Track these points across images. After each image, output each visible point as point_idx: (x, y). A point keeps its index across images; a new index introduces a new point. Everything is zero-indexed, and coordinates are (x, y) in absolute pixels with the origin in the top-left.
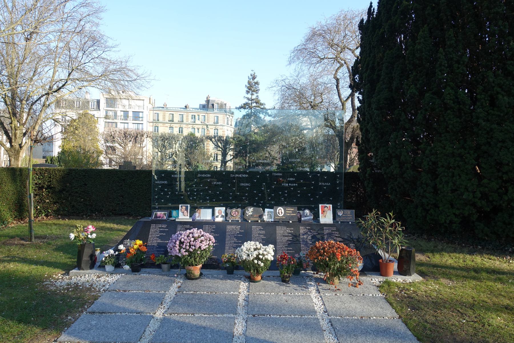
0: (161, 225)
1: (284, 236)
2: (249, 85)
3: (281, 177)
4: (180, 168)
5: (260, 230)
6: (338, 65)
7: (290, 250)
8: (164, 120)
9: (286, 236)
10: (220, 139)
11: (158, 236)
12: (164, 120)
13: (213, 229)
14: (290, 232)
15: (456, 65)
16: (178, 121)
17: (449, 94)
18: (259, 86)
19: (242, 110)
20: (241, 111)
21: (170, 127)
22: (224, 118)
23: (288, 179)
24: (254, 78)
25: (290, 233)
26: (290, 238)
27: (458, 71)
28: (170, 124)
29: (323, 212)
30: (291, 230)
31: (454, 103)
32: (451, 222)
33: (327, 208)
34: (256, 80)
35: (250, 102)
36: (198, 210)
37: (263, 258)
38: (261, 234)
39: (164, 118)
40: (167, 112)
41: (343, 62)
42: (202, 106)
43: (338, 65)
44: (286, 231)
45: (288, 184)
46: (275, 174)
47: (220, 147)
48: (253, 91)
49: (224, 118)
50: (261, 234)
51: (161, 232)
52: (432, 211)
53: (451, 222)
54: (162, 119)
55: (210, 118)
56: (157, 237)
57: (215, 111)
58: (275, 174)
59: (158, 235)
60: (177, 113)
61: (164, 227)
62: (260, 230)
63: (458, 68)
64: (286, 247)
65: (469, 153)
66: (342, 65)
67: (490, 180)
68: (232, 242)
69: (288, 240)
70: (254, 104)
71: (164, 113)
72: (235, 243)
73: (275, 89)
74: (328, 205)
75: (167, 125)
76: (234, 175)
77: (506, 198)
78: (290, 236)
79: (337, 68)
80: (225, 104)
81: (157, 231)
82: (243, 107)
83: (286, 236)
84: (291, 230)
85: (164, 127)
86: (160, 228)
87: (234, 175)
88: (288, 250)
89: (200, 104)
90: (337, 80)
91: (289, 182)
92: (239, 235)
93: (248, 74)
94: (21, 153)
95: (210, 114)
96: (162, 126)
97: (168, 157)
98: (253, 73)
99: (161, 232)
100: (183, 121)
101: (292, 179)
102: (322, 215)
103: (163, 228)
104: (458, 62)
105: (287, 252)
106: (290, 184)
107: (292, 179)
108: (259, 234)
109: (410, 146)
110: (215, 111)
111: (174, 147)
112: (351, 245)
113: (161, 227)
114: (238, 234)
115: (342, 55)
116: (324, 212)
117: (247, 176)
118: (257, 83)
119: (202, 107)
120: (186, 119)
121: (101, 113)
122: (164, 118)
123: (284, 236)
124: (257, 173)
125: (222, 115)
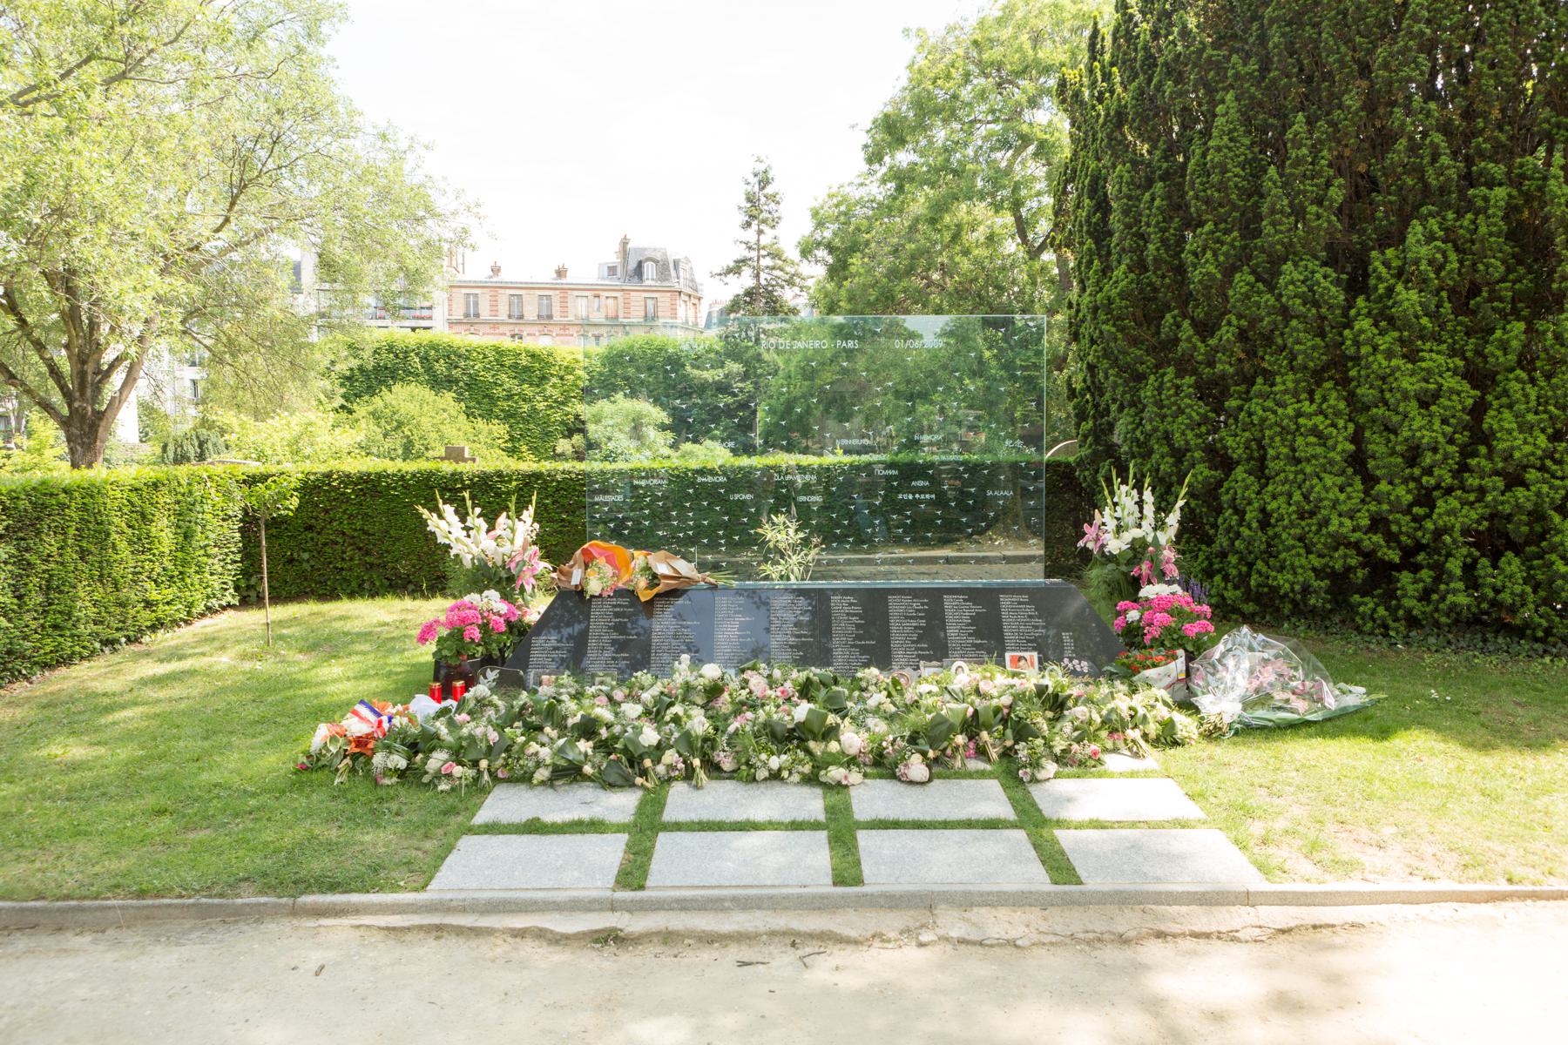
1: (906, 617)
2: (749, 205)
4: (1308, 460)
5: (850, 604)
9: (912, 618)
13: (740, 605)
15: (1313, 209)
16: (539, 316)
17: (1292, 282)
18: (781, 207)
19: (731, 278)
24: (764, 182)
26: (923, 623)
27: (1316, 223)
30: (922, 604)
31: (1304, 304)
32: (1306, 589)
34: (769, 190)
35: (754, 254)
40: (502, 291)
42: (606, 270)
48: (764, 221)
51: (617, 615)
52: (1260, 565)
53: (1306, 589)
56: (610, 628)
60: (532, 292)
62: (850, 604)
63: (1318, 217)
64: (913, 642)
65: (1334, 425)
67: (1391, 483)
69: (916, 627)
70: (767, 262)
75: (502, 329)
77: (1429, 525)
78: (921, 618)
80: (676, 264)
82: (736, 269)
83: (912, 618)
84: (922, 604)
86: (614, 606)
91: (915, 491)
93: (747, 169)
94: (101, 429)
98: (761, 168)
99: (617, 615)
100: (550, 317)
101: (920, 483)
103: (620, 606)
104: (1319, 202)
107: (920, 483)
108: (848, 614)
118: (773, 198)
119: (606, 273)
123: (906, 617)
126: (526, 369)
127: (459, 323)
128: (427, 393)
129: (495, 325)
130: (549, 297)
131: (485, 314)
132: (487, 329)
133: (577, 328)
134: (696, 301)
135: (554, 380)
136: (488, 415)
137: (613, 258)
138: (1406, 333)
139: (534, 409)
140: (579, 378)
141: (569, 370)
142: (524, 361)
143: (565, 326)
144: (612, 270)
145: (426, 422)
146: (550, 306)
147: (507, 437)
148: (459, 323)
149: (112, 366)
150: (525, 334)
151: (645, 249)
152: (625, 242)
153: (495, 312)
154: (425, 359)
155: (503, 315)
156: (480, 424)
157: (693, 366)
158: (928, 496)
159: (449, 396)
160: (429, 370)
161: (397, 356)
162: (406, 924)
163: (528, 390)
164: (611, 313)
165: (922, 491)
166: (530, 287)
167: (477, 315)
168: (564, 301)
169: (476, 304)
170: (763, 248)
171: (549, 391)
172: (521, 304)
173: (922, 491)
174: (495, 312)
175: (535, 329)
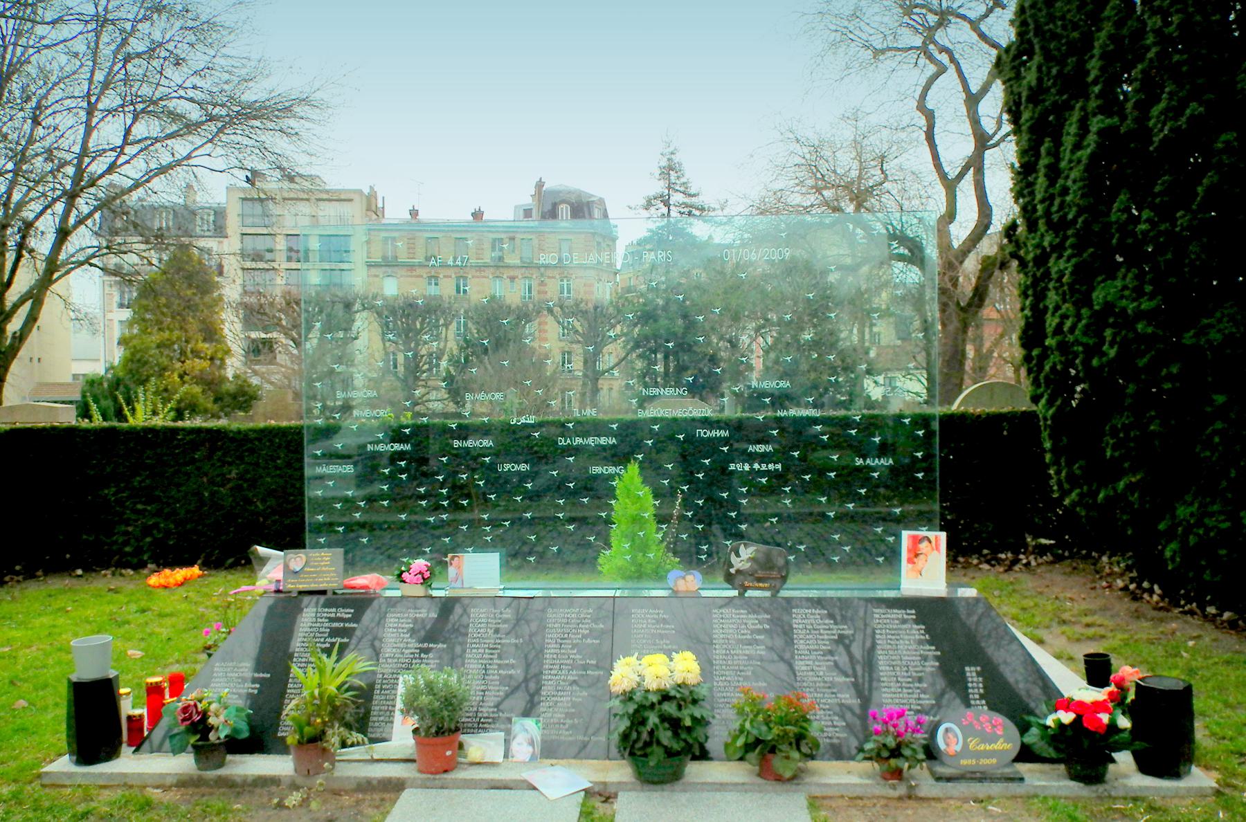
0: (334, 610)
3: (726, 441)
6: (931, 69)
8: (411, 256)
10: (577, 310)
11: (324, 646)
12: (411, 256)
21: (430, 277)
25: (759, 632)
29: (915, 554)
33: (930, 542)
36: (453, 558)
37: (416, 680)
38: (661, 637)
41: (944, 58)
42: (522, 213)
43: (931, 69)
44: (746, 624)
46: (705, 433)
47: (576, 332)
50: (661, 637)
58: (705, 433)
59: (325, 643)
66: (942, 70)
68: (566, 665)
69: (750, 658)
73: (16, 594)
74: (932, 535)
75: (419, 271)
76: (568, 441)
78: (757, 642)
79: (987, 46)
81: (323, 630)
85: (411, 276)
87: (568, 441)
89: (516, 207)
90: (930, 116)
91: (751, 458)
92: (589, 641)
97: (426, 367)
101: (760, 448)
102: (910, 566)
106: (756, 466)
107: (760, 448)
111: (443, 335)
112: (967, 669)
113: (333, 615)
114: (584, 637)
115: (940, 36)
116: (917, 555)
117: (613, 441)
121: (232, 244)
127: (377, 265)
133: (492, 270)
134: (611, 243)
137: (527, 199)
138: (1198, 18)
144: (528, 213)
148: (377, 265)
149: (16, 307)
150: (441, 276)
151: (560, 192)
152: (540, 185)
158: (771, 467)
162: (885, 591)
165: (764, 458)
170: (140, 97)
173: (764, 458)
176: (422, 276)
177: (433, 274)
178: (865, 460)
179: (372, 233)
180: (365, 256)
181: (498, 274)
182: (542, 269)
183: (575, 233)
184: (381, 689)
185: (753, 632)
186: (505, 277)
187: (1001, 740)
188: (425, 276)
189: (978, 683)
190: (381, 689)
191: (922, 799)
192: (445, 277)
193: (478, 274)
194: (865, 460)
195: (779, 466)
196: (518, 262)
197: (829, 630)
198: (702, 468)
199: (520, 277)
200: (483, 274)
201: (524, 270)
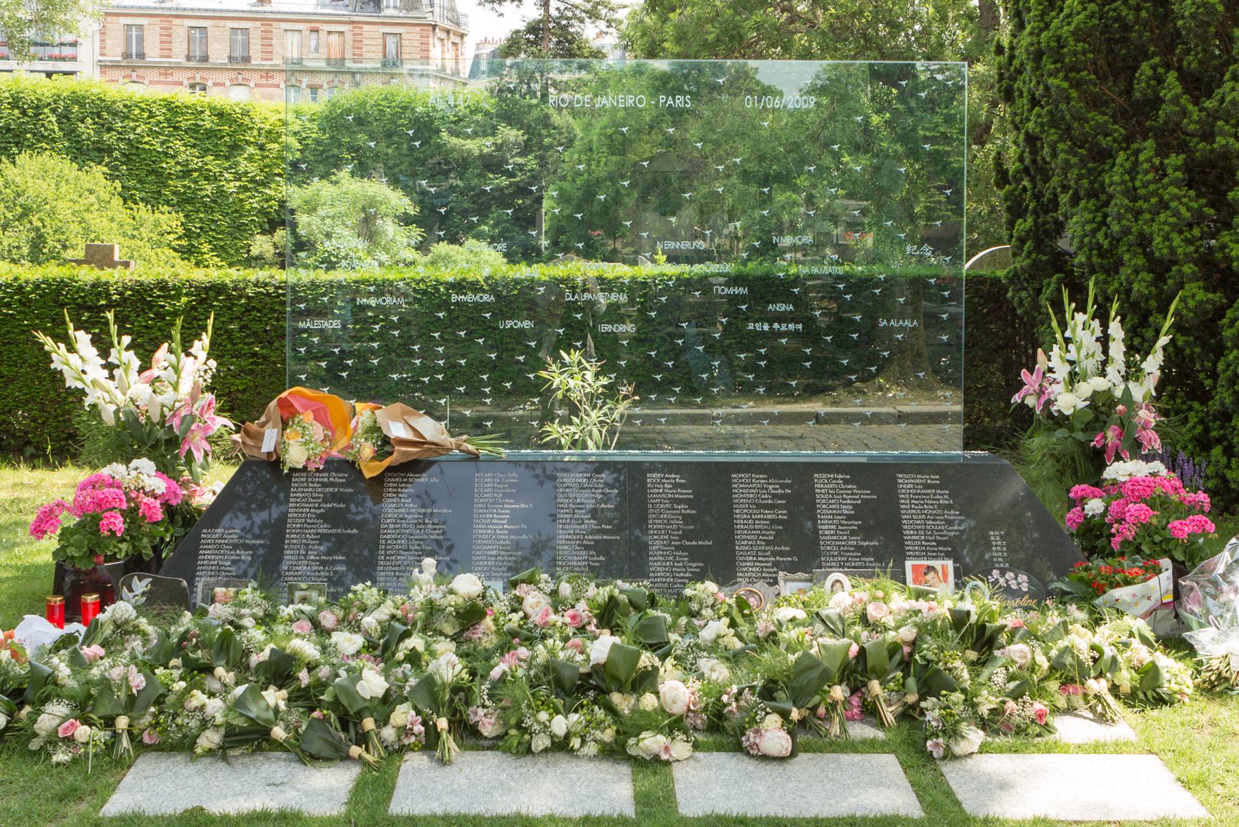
1: (759, 506)
3: (743, 299)
5: (676, 486)
7: (782, 554)
8: (166, 53)
11: (319, 511)
12: (166, 53)
13: (511, 485)
14: (780, 491)
16: (230, 58)
20: (501, 15)
22: (425, 40)
23: (770, 307)
26: (782, 514)
28: (190, 74)
30: (783, 486)
38: (679, 501)
39: (166, 46)
40: (178, 21)
45: (771, 325)
49: (425, 40)
50: (679, 501)
54: (157, 51)
55: (365, 42)
57: (387, 12)
60: (221, 23)
61: (337, 480)
62: (676, 486)
64: (768, 543)
69: (773, 522)
71: (165, 25)
72: (593, 532)
75: (177, 76)
78: (779, 507)
85: (166, 83)
86: (324, 485)
88: (774, 554)
95: (366, 27)
96: (157, 83)
100: (247, 59)
101: (781, 307)
103: (332, 485)
105: (772, 559)
107: (781, 307)
109: (1185, 200)
110: (387, 12)
112: (991, 533)
113: (325, 480)
120: (259, 48)
122: (166, 46)
123: (759, 506)
124: (969, 336)
125: (418, 29)
126: (210, 134)
127: (115, 66)
128: (68, 168)
129: (167, 70)
130: (245, 31)
131: (153, 53)
132: (154, 75)
134: (457, 40)
135: (251, 150)
136: (154, 200)
139: (221, 192)
140: (287, 148)
141: (272, 135)
142: (208, 122)
143: (267, 73)
145: (64, 209)
146: (247, 44)
147: (180, 231)
148: (115, 66)
150: (210, 83)
153: (166, 49)
154: (64, 118)
155: (179, 57)
156: (143, 211)
157: (453, 133)
158: (791, 326)
159: (99, 171)
160: (70, 134)
161: (24, 113)
163: (210, 161)
164: (335, 54)
165: (781, 318)
166: (220, 17)
167: (141, 56)
168: (266, 38)
169: (140, 40)
171: (244, 165)
172: (205, 40)
173: (781, 318)
174: (166, 49)
175: (224, 77)
176: (181, 83)
177: (198, 80)
178: (889, 321)
179: (109, 19)
180: (97, 51)
181: (293, 81)
182: (358, 77)
183: (353, 22)
184: (386, 555)
185: (774, 496)
186: (303, 86)
187: (1027, 597)
188: (186, 83)
189: (1002, 546)
190: (386, 555)
191: (765, 758)
192: (215, 84)
193: (264, 81)
194: (889, 321)
195: (800, 327)
196: (322, 65)
197: (852, 497)
198: (346, 368)
199: (325, 86)
200: (271, 81)
201: (331, 77)
